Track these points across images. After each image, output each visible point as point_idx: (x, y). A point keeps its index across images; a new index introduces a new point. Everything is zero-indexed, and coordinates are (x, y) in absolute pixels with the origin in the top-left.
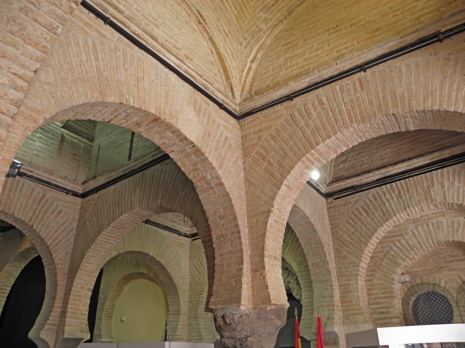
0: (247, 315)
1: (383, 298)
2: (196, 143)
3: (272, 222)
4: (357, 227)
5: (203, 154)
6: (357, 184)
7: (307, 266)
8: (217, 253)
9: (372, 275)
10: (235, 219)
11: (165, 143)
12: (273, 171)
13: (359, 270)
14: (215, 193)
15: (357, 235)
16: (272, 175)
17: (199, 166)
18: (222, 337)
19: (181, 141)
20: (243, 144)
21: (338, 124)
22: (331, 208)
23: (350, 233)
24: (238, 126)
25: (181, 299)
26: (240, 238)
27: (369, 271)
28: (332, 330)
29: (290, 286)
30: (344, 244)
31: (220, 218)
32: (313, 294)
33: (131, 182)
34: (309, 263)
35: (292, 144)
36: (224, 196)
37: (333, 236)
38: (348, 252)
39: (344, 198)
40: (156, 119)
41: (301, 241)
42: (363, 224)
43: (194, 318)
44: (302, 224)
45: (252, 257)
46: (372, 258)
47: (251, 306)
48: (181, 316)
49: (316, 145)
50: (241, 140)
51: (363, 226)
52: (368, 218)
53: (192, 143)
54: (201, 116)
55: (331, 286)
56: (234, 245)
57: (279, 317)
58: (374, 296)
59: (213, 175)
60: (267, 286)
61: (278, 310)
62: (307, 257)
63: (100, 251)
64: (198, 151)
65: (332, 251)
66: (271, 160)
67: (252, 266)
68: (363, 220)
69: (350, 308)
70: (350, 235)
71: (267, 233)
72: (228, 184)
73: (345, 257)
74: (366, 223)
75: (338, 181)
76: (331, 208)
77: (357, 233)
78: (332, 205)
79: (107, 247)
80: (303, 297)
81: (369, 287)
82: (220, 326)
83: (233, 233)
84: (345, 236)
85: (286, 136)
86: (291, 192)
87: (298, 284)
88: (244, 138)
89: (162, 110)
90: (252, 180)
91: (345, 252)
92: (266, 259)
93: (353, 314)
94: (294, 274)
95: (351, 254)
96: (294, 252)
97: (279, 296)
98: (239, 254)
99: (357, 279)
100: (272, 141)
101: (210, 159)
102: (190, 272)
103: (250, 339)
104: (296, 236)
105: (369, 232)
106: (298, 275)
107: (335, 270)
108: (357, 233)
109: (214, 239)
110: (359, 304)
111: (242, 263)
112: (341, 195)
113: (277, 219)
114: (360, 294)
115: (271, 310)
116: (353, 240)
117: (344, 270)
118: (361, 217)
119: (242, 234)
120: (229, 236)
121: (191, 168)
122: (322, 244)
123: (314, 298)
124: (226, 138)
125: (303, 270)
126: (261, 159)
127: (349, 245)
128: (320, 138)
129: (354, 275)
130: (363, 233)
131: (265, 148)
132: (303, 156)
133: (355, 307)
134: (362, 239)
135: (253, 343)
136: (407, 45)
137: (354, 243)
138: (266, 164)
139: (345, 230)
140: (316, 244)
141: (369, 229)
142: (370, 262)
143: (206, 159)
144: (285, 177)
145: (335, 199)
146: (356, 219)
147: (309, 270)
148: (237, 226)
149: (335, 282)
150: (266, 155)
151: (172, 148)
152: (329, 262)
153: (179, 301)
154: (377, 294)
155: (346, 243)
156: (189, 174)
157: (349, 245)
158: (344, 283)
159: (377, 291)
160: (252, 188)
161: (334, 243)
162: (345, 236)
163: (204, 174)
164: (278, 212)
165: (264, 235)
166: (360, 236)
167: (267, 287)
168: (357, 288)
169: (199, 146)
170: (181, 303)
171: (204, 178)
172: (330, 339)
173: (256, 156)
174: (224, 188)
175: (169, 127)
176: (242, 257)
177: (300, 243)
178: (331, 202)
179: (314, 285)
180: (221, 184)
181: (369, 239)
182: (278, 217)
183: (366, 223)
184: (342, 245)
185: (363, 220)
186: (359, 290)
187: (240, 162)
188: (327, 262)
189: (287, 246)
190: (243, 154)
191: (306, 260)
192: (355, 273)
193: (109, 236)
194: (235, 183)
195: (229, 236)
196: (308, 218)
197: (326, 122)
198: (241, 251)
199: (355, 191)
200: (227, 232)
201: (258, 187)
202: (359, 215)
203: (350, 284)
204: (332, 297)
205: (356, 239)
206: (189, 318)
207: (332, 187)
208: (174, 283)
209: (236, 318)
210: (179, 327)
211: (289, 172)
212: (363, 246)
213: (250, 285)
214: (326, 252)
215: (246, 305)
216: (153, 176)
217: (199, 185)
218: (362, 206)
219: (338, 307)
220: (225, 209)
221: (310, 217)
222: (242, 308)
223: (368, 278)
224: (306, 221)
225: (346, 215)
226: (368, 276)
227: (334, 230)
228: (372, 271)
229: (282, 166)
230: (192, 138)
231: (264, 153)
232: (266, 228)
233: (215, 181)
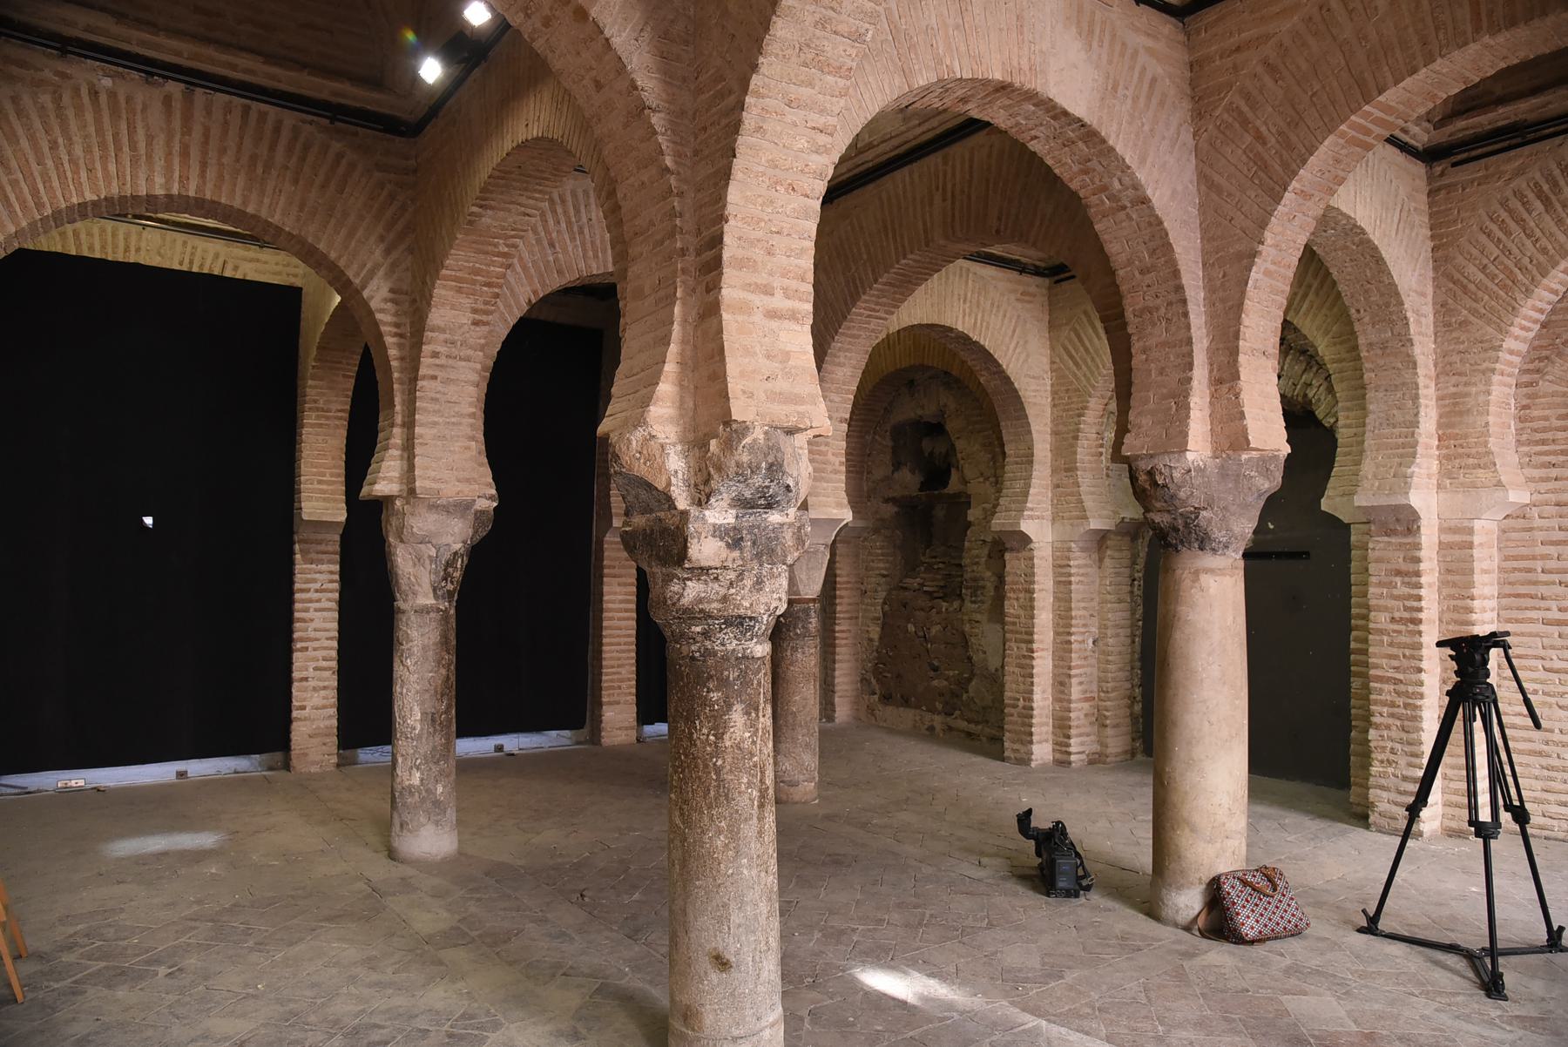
0: (1199, 470)
1: (1558, 429)
2: (1087, 120)
3: (1260, 276)
4: (1510, 245)
5: (1104, 141)
6: (1531, 117)
7: (1355, 348)
8: (1136, 347)
9: (1538, 371)
10: (1176, 273)
11: (1018, 124)
12: (1266, 157)
13: (1497, 360)
14: (1130, 218)
15: (1506, 267)
16: (1265, 167)
17: (1094, 164)
18: (1147, 510)
19: (1054, 118)
20: (1193, 84)
21: (1441, 36)
22: (1439, 189)
23: (1485, 261)
24: (1182, 37)
25: (1034, 428)
26: (1186, 315)
27: (1532, 361)
28: (1401, 501)
29: (1310, 395)
30: (1465, 290)
31: (1142, 272)
32: (1365, 416)
33: (916, 176)
34: (1361, 341)
35: (1317, 87)
36: (1150, 224)
37: (1435, 269)
38: (1474, 312)
39: (1483, 161)
40: (1003, 88)
41: (1341, 287)
42: (1529, 236)
43: (1067, 470)
44: (1347, 247)
45: (1212, 353)
46: (1544, 325)
47: (1209, 453)
48: (1036, 466)
49: (1375, 93)
50: (1188, 74)
51: (1528, 243)
52: (1547, 218)
53: (1080, 120)
54: (1095, 45)
55: (1416, 398)
56: (1173, 329)
57: (1266, 473)
58: (1535, 425)
59: (1126, 180)
60: (1242, 413)
61: (1264, 463)
62: (1357, 327)
63: (858, 337)
64: (1090, 135)
65: (1428, 310)
66: (1263, 129)
67: (1211, 371)
68: (1532, 224)
69: (1460, 450)
70: (1485, 267)
71: (1247, 302)
72: (1159, 197)
73: (1464, 324)
74: (1538, 233)
75: (1467, 111)
76: (1439, 189)
77: (1506, 261)
78: (1446, 181)
79: (872, 326)
80: (1340, 423)
81: (1525, 402)
82: (1144, 490)
83: (1170, 304)
84: (1471, 269)
85: (1304, 66)
86: (1308, 204)
87: (1331, 390)
88: (1196, 68)
89: (1015, 63)
90: (1217, 178)
91: (1465, 312)
92: (1242, 358)
93: (1467, 467)
94: (1321, 366)
95: (1481, 317)
96: (1324, 311)
97: (1269, 433)
98: (1185, 349)
99: (1488, 383)
100: (1267, 79)
101: (1119, 149)
102: (1053, 363)
103: (1204, 513)
104: (1328, 274)
105: (1542, 258)
106: (1331, 367)
107: (1432, 357)
108: (1506, 261)
109: (1129, 315)
110: (1486, 442)
111: (1190, 366)
112: (1474, 153)
113: (1273, 268)
114: (1491, 419)
115: (1250, 459)
116: (1493, 280)
117: (1456, 358)
118: (1525, 216)
119: (1191, 307)
120: (1163, 310)
121: (1075, 168)
122: (1398, 294)
123: (1369, 427)
124: (1154, 80)
125: (1345, 355)
126: (1237, 125)
127: (1480, 294)
128: (1388, 74)
129: (1484, 373)
130: (1526, 261)
131: (1247, 97)
132: (1342, 122)
133: (1474, 451)
134: (1520, 277)
135: (1210, 521)
136: (1160, 609)
137: (1496, 289)
138: (1248, 139)
139: (1475, 252)
140: (1382, 295)
141: (1544, 251)
142: (1538, 337)
143: (1112, 149)
144: (1295, 173)
145: (1454, 165)
146: (1509, 221)
147: (1358, 358)
148: (1180, 288)
149: (1427, 387)
150: (1250, 115)
151: (1033, 133)
152: (1416, 339)
153: (1030, 432)
154: (1546, 418)
155: (1472, 287)
156: (1071, 180)
157: (1480, 294)
158: (1453, 390)
159: (1547, 412)
160: (1214, 196)
161: (1437, 287)
162: (1471, 269)
163: (1106, 180)
164: (1273, 251)
165: (1239, 307)
166: (1516, 270)
167: (1242, 415)
168: (1488, 403)
169: (1095, 125)
170: (1035, 435)
171: (1104, 189)
172: (1398, 520)
173: (1226, 116)
174: (1152, 209)
175: (1031, 96)
176: (1190, 354)
177: (1339, 293)
178: (1442, 174)
179: (1370, 395)
180: (1145, 201)
181: (1539, 277)
182: (1274, 263)
183: (1538, 233)
184: (1459, 292)
185: (1532, 224)
186: (1492, 409)
187: (1187, 137)
188: (1410, 340)
189: (1305, 296)
190: (1192, 110)
191: (1353, 333)
192: (1485, 365)
193: (877, 304)
194: (1174, 191)
195: (1163, 310)
196: (1363, 232)
197: (1411, 30)
198: (1189, 342)
199: (1519, 140)
200: (1158, 301)
201: (1229, 195)
202: (1521, 209)
203: (1467, 395)
204: (1415, 424)
205: (1502, 276)
206: (1054, 471)
207: (1450, 129)
208: (1016, 391)
209: (1176, 474)
210: (1032, 491)
211: (1304, 162)
212: (1519, 296)
213: (1207, 412)
214: (1409, 314)
215: (1199, 447)
216: (971, 160)
217: (1097, 204)
218: (1536, 184)
219: (1428, 447)
220: (1153, 253)
221: (1368, 229)
222: (1190, 456)
223: (1526, 378)
224: (1356, 239)
225: (1481, 211)
226: (1528, 371)
227: (1440, 254)
228: (1540, 359)
229: (1290, 147)
230: (1078, 108)
231: (1245, 109)
232: (1243, 293)
233: (1131, 192)
